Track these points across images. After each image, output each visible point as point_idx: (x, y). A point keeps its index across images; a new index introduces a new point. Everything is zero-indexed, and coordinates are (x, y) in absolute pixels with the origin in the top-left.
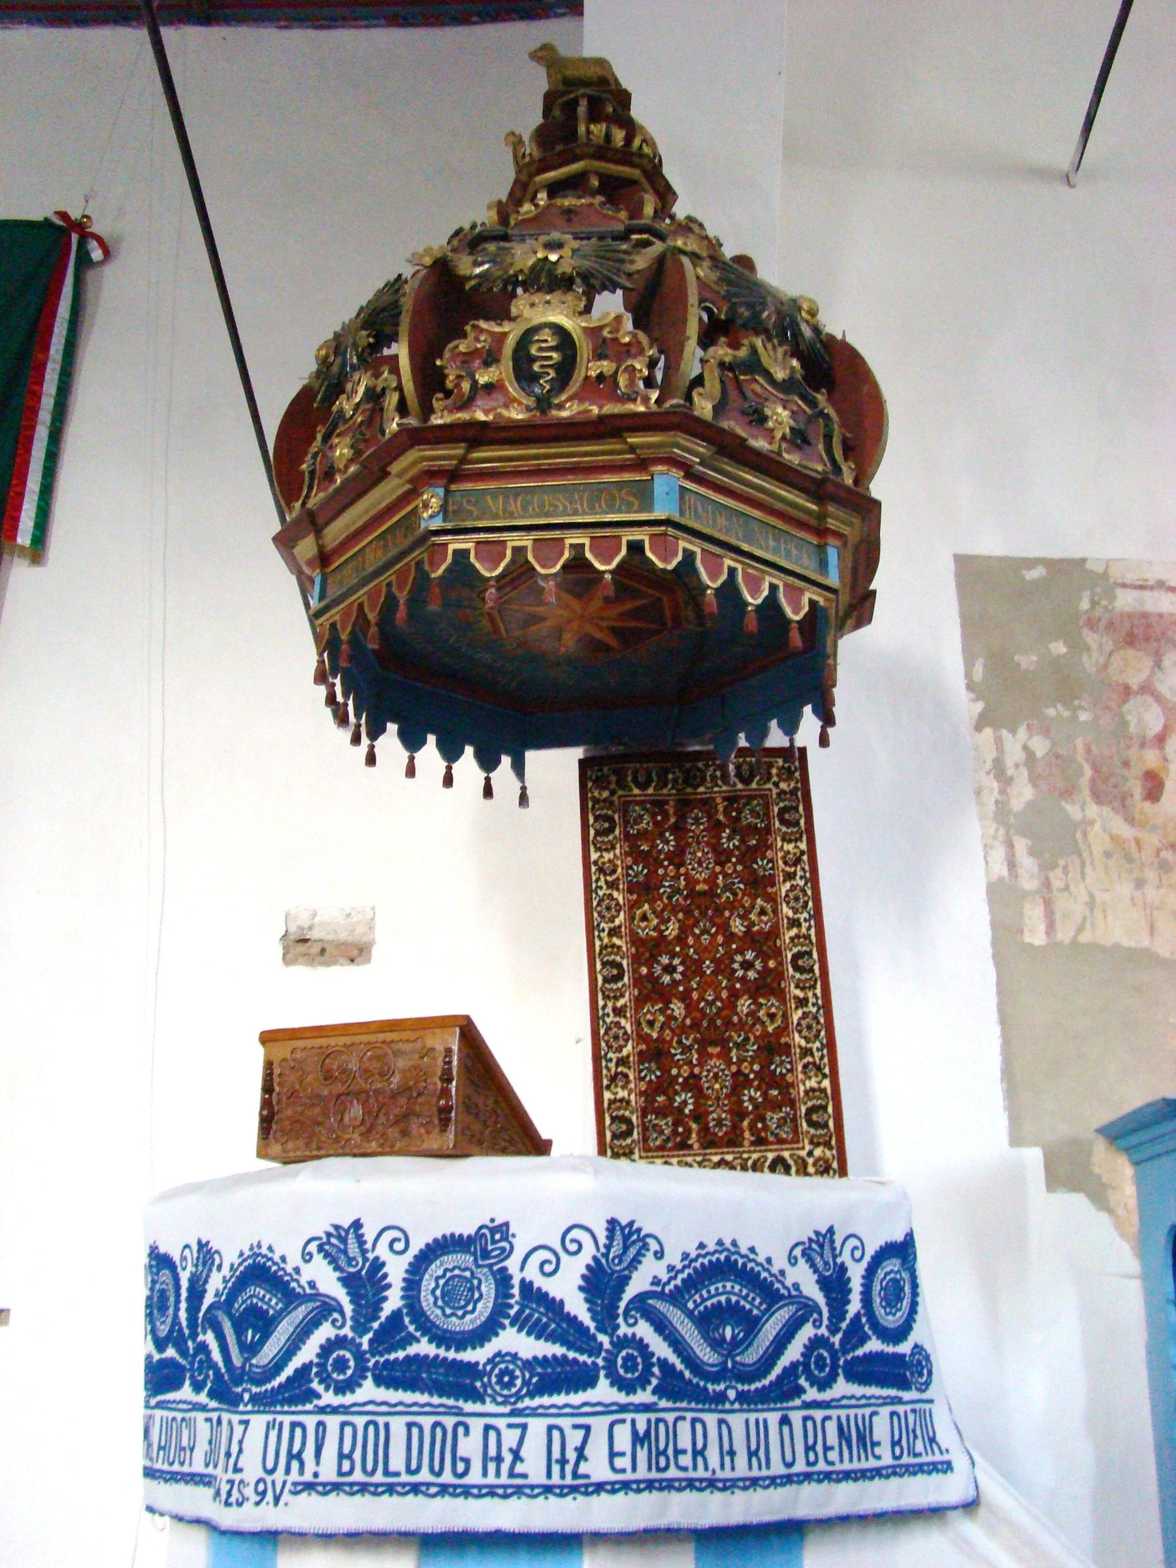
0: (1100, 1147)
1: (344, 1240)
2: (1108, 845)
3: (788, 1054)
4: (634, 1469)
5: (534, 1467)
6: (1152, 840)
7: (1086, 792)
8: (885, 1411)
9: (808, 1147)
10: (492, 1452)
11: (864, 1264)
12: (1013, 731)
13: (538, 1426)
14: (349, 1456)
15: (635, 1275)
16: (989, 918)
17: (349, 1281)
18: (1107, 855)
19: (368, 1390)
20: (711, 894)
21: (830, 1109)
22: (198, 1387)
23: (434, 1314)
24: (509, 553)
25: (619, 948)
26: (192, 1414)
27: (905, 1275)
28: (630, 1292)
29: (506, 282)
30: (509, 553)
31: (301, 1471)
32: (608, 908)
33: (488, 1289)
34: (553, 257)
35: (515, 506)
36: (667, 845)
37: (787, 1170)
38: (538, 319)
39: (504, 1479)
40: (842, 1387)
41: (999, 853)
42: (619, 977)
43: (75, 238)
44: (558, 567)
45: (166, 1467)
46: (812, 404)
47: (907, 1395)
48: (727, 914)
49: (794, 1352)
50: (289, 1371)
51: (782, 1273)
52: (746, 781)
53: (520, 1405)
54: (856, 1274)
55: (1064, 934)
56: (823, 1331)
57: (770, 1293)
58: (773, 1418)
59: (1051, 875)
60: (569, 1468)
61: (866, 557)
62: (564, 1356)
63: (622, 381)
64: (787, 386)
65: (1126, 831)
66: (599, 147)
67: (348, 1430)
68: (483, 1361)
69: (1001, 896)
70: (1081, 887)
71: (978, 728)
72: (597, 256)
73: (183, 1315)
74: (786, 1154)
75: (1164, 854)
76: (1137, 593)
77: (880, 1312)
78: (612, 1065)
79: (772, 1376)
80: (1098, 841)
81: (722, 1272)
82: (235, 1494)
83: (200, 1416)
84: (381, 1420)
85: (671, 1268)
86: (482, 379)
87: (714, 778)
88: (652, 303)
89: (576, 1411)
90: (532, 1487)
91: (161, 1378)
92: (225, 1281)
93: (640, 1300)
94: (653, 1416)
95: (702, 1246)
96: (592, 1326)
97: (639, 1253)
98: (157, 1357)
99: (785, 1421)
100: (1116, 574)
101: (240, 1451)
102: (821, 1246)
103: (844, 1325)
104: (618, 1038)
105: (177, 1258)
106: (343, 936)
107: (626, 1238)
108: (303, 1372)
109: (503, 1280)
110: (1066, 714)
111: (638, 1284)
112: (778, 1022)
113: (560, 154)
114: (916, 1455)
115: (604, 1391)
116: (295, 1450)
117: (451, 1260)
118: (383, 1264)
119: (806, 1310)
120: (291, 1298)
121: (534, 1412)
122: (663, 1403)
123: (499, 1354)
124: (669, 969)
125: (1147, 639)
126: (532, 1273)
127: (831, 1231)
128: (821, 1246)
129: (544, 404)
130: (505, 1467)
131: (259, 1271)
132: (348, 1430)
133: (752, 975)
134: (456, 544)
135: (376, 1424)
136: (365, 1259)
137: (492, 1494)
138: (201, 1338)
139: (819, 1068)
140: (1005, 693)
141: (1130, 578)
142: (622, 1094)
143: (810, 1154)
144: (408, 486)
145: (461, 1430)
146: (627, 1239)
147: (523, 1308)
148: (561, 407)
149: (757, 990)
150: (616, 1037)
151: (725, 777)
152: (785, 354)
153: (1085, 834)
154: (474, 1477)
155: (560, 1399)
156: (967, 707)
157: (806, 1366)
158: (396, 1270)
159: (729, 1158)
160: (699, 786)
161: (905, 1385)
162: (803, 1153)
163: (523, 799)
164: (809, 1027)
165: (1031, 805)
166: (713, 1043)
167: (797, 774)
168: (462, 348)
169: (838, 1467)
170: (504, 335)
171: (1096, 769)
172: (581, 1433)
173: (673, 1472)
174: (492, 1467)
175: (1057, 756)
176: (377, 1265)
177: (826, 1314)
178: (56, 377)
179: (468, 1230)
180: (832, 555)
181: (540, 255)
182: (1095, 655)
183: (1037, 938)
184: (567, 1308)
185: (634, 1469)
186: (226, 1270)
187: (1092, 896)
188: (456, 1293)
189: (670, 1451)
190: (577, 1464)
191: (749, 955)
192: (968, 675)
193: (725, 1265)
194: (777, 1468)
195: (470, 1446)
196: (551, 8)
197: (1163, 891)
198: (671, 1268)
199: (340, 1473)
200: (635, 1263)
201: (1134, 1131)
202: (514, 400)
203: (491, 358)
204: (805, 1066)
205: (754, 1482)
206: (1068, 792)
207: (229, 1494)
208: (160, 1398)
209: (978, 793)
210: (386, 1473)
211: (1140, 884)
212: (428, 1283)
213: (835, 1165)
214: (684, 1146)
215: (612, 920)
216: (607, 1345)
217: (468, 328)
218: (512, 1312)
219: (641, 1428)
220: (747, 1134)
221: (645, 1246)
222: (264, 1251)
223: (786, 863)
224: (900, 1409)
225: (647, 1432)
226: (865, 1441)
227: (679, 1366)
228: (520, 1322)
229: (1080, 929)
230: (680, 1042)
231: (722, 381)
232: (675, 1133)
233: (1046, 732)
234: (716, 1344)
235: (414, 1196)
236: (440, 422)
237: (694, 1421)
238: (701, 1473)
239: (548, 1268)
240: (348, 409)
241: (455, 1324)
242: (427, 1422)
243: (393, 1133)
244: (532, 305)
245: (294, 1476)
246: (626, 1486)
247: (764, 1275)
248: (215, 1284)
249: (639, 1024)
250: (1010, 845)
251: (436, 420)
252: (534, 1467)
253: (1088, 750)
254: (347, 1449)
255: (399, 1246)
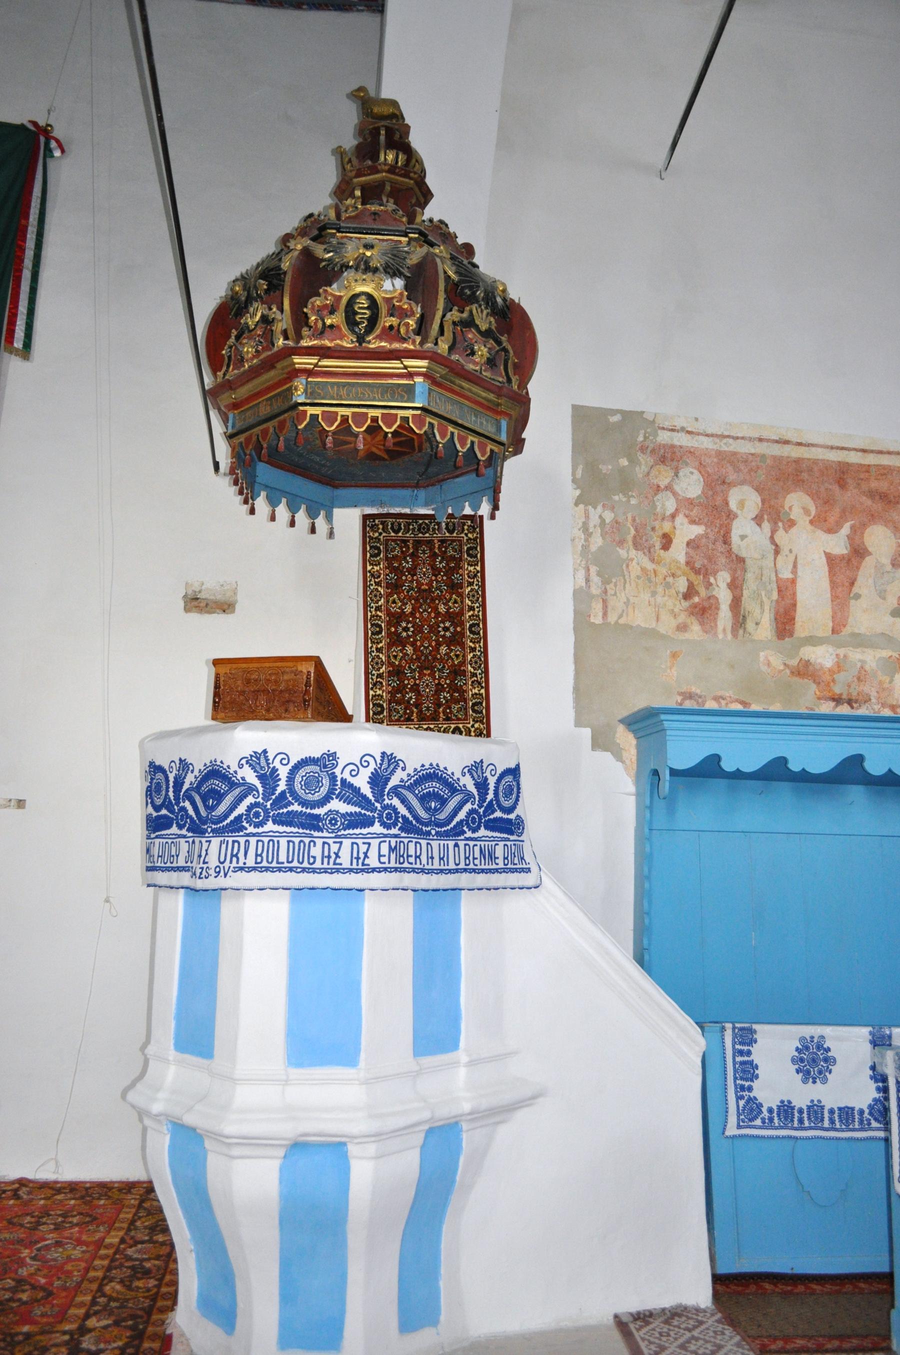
0: (621, 728)
1: (259, 759)
2: (639, 573)
3: (465, 676)
4: (389, 863)
5: (345, 860)
6: (662, 571)
7: (630, 543)
8: (501, 844)
9: (472, 723)
10: (326, 854)
11: (496, 777)
12: (595, 508)
13: (347, 843)
14: (261, 855)
15: (393, 777)
16: (573, 608)
17: (261, 777)
18: (638, 577)
19: (270, 826)
20: (429, 591)
21: (484, 704)
22: (180, 827)
23: (301, 793)
24: (339, 418)
25: (380, 617)
26: (178, 840)
27: (514, 783)
28: (391, 784)
29: (342, 266)
30: (339, 418)
31: (238, 862)
32: (376, 596)
33: (326, 782)
34: (368, 254)
35: (343, 392)
36: (408, 564)
37: (461, 733)
38: (360, 289)
39: (331, 866)
40: (483, 832)
41: (581, 574)
42: (380, 632)
43: (42, 139)
44: (364, 428)
45: (163, 865)
46: (499, 343)
47: (512, 838)
48: (437, 602)
49: (462, 815)
50: (231, 818)
51: (458, 779)
52: (451, 532)
53: (339, 833)
54: (492, 781)
55: (612, 618)
56: (475, 806)
57: (453, 789)
58: (451, 844)
59: (608, 587)
60: (360, 861)
61: (522, 421)
62: (360, 812)
63: (402, 330)
64: (487, 334)
65: (650, 566)
66: (391, 166)
67: (260, 844)
68: (323, 813)
69: (581, 596)
70: (623, 594)
71: (576, 504)
72: (393, 255)
73: (171, 794)
74: (461, 726)
75: (667, 579)
76: (669, 433)
77: (502, 799)
78: (374, 677)
79: (452, 825)
80: (635, 569)
81: (432, 778)
82: (204, 873)
83: (183, 840)
84: (276, 839)
85: (409, 775)
86: (329, 322)
87: (434, 529)
88: (419, 282)
89: (364, 837)
90: (344, 869)
91: (155, 825)
92: (196, 777)
93: (395, 788)
94: (398, 840)
95: (423, 766)
96: (373, 799)
97: (395, 768)
98: (155, 814)
99: (456, 845)
100: (659, 422)
101: (207, 854)
102: (477, 768)
103: (485, 804)
104: (378, 664)
105: (166, 767)
106: (219, 597)
107: (389, 761)
108: (239, 818)
109: (333, 778)
110: (624, 500)
111: (394, 781)
112: (460, 659)
113: (369, 167)
114: (515, 864)
115: (377, 828)
116: (235, 853)
117: (308, 769)
118: (277, 770)
119: (469, 797)
120: (233, 785)
121: (345, 837)
122: (403, 835)
123: (330, 811)
124: (406, 629)
125: (672, 460)
126: (346, 775)
127: (482, 761)
128: (477, 768)
129: (361, 339)
130: (332, 861)
131: (215, 772)
132: (260, 844)
133: (448, 634)
134: (311, 411)
135: (273, 841)
136: (269, 768)
137: (326, 872)
138: (182, 804)
139: (480, 683)
140: (593, 485)
141: (667, 424)
142: (379, 692)
143: (473, 726)
144: (285, 376)
145: (312, 844)
146: (390, 761)
147: (342, 790)
148: (369, 342)
149: (450, 642)
150: (377, 663)
151: (439, 529)
152: (488, 314)
153: (627, 566)
154: (318, 864)
155: (357, 831)
156: (571, 492)
157: (467, 821)
158: (283, 773)
159: (432, 726)
160: (426, 533)
161: (512, 833)
162: (469, 726)
163: (331, 535)
164: (476, 662)
165: (600, 548)
166: (427, 669)
167: (478, 530)
168: (318, 303)
169: (479, 867)
170: (340, 297)
171: (636, 530)
172: (367, 846)
173: (406, 865)
174: (326, 860)
175: (617, 522)
176: (275, 770)
177: (477, 799)
178: (34, 237)
179: (317, 755)
180: (504, 424)
181: (361, 251)
182: (643, 467)
183: (597, 619)
184: (362, 791)
185: (389, 863)
186: (196, 773)
187: (628, 600)
188: (311, 783)
189: (405, 856)
190: (364, 859)
191: (448, 624)
192: (574, 474)
193: (432, 775)
194: (452, 866)
195: (316, 851)
196: (355, 6)
197: (666, 598)
198: (409, 775)
199: (256, 863)
200: (393, 772)
201: (635, 723)
202: (345, 336)
203: (332, 311)
204: (473, 682)
205: (442, 871)
206: (621, 543)
207: (201, 873)
208: (157, 833)
209: (573, 540)
210: (278, 863)
211: (654, 594)
212: (298, 779)
213: (485, 732)
214: (409, 719)
215: (377, 602)
216: (379, 808)
217: (321, 291)
218: (337, 792)
219: (393, 845)
220: (441, 715)
221: (398, 765)
222: (218, 763)
223: (469, 577)
224: (509, 843)
225: (396, 847)
226: (492, 857)
227: (411, 819)
228: (340, 797)
229: (620, 616)
230: (410, 667)
231: (454, 333)
232: (405, 713)
233: (612, 509)
234: (427, 810)
235: (290, 741)
236: (305, 344)
237: (416, 843)
238: (418, 866)
239: (354, 773)
240: (251, 323)
241: (310, 797)
242: (297, 840)
243: (281, 710)
244: (356, 281)
245: (234, 864)
246: (385, 869)
247: (450, 780)
248: (190, 779)
249: (389, 657)
250: (588, 570)
251: (304, 343)
252: (345, 860)
253: (634, 520)
254: (259, 852)
255: (285, 762)
